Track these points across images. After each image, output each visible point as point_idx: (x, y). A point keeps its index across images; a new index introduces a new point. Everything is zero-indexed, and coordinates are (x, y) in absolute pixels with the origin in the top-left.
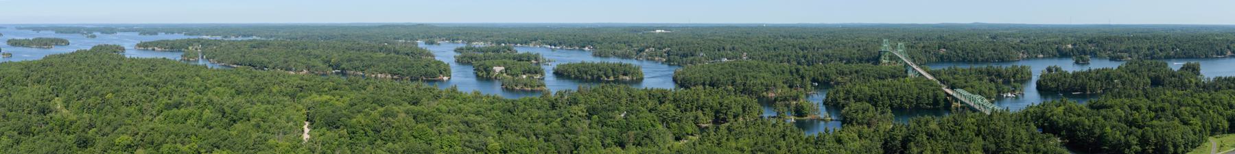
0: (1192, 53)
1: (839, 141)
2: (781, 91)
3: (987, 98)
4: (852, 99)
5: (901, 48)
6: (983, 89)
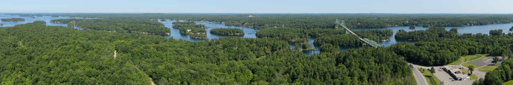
0: (455, 24)
1: (319, 58)
2: (297, 39)
3: (376, 42)
4: (324, 42)
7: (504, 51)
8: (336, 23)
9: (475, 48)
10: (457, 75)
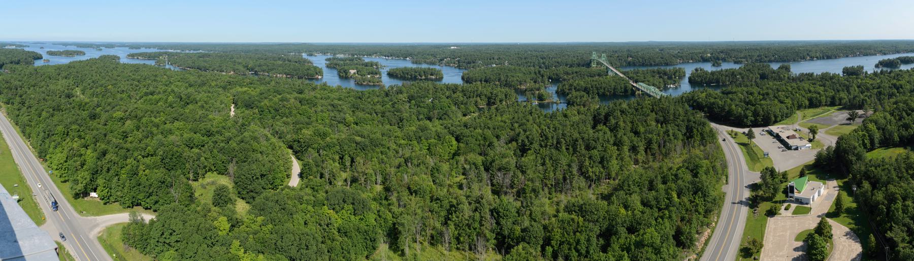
0: (785, 58)
1: (565, 116)
2: (529, 85)
3: (658, 88)
5: (604, 57)
6: (655, 82)
7: (866, 100)
8: (592, 58)
9: (820, 97)
10: (790, 142)
